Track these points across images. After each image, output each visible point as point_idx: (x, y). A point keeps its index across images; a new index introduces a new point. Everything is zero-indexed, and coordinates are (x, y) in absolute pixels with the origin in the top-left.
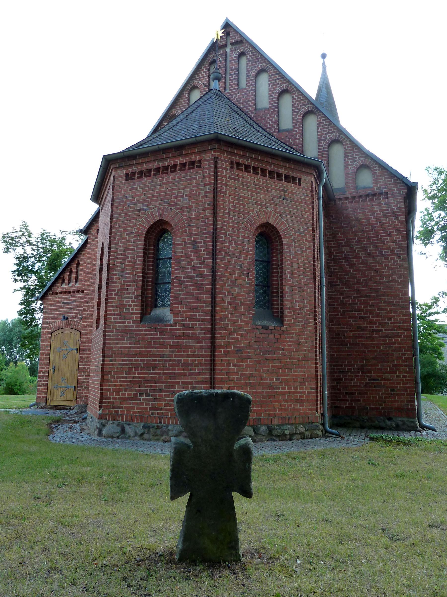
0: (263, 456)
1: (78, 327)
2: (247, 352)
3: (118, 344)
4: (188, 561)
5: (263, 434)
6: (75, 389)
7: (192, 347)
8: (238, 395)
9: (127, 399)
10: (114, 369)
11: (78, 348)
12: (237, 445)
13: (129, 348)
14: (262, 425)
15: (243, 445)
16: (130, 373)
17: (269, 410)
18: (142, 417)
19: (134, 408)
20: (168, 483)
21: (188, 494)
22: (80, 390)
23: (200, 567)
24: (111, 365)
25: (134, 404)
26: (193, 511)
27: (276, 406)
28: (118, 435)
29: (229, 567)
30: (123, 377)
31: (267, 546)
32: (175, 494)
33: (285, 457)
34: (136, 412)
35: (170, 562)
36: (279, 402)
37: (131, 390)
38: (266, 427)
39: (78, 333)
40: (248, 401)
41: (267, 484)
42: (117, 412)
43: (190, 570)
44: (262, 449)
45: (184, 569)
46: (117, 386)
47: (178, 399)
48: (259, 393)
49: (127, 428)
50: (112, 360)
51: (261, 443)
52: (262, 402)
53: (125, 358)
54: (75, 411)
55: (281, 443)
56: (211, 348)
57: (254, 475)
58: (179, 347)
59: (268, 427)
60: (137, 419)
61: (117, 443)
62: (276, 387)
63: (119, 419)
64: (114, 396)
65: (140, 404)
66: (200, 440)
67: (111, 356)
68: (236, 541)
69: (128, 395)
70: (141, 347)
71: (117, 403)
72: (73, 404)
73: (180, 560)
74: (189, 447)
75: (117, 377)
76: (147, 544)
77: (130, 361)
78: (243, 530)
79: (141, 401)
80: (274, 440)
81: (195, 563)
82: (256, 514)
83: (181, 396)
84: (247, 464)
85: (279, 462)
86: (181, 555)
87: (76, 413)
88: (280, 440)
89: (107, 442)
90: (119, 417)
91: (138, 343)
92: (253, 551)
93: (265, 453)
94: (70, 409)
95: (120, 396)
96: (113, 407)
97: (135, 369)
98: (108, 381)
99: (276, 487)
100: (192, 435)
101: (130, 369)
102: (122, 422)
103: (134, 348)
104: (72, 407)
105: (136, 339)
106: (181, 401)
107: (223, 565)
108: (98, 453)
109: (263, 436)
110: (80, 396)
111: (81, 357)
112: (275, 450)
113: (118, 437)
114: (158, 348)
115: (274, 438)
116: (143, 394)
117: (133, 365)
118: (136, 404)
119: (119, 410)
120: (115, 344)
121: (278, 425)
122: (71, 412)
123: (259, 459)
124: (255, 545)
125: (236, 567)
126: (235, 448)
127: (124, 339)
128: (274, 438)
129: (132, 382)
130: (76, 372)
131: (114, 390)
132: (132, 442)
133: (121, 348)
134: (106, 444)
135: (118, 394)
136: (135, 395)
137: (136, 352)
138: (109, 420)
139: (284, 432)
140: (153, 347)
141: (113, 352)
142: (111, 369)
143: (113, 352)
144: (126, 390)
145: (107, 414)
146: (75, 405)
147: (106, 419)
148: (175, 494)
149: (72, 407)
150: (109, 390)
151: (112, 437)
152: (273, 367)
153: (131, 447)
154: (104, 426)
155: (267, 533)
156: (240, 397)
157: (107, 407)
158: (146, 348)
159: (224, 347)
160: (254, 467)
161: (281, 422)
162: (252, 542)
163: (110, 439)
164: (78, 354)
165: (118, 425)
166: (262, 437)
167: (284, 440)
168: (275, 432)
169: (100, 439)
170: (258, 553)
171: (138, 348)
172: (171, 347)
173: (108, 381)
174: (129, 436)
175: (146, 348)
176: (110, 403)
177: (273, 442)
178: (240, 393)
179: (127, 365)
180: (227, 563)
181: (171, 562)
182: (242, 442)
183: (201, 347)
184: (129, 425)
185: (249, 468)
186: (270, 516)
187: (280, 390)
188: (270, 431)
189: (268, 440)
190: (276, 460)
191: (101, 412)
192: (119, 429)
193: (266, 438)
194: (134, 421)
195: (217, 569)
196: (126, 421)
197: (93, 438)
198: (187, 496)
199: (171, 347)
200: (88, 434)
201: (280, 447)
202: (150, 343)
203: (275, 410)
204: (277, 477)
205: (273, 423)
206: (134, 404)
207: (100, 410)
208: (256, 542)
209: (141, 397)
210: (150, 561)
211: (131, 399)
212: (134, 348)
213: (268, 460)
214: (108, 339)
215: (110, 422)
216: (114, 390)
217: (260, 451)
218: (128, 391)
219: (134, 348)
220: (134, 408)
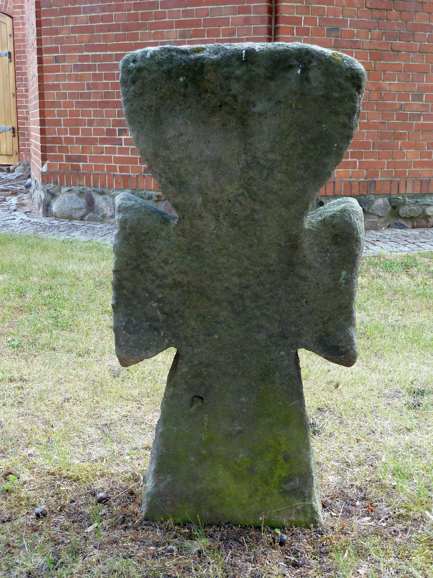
0: (379, 257)
1: (6, 7)
2: (352, 34)
3: (67, 21)
4: (170, 522)
5: (380, 214)
6: (14, 132)
7: (225, 22)
8: (319, 57)
9: (93, 141)
10: (64, 77)
11: (12, 51)
12: (312, 219)
13: (89, 30)
14: (378, 195)
15: (333, 217)
16: (95, 86)
17: (394, 165)
18: (126, 179)
19: (108, 160)
20: (108, 320)
21: (172, 352)
22: (23, 134)
23: (201, 543)
24: (57, 69)
25: (109, 150)
26: (186, 395)
27: (411, 155)
28: (81, 213)
29: (282, 543)
30: (82, 95)
31: (389, 480)
32: (132, 346)
33: (427, 260)
34: (114, 169)
35: (123, 521)
36: (417, 147)
37: (102, 123)
38: (386, 199)
39: (8, 20)
40: (355, 79)
41: (386, 317)
42: (77, 168)
43: (171, 551)
44: (376, 243)
45: (157, 545)
46: (72, 113)
47: (127, 71)
48: (374, 126)
49: (99, 200)
50: (57, 60)
51: (374, 232)
52: (381, 146)
53: (85, 53)
54: (17, 173)
55: (416, 232)
56: (270, 22)
57: (360, 296)
58: (197, 23)
59: (390, 200)
60: (117, 183)
61: (77, 228)
62: (413, 115)
63: (81, 184)
64: (68, 136)
65: (122, 151)
66: (199, 200)
67: (56, 50)
68: (306, 477)
69: (97, 132)
70: (117, 28)
71: (76, 150)
72: (13, 161)
73: (149, 520)
74: (165, 220)
75: (72, 96)
76: (77, 464)
77: (95, 58)
78: (329, 429)
79: (124, 146)
80: (402, 227)
81: (186, 528)
82: (361, 388)
83: (134, 61)
84: (344, 273)
85: (414, 271)
86: (151, 506)
87: (18, 178)
88: (414, 227)
89: (58, 227)
90: (81, 179)
91: (109, 18)
92: (352, 493)
93: (384, 252)
94: (9, 171)
95: (80, 136)
96: (69, 159)
97: (107, 77)
98: (53, 104)
99: (408, 323)
100: (174, 183)
101: (97, 77)
102: (89, 189)
103: (101, 31)
104: (11, 168)
105: (103, 9)
106: (137, 77)
107: (266, 537)
108: (32, 247)
109: (379, 217)
110: (24, 145)
111: (18, 69)
112: (405, 245)
113: (82, 219)
114: (152, 26)
115: (403, 222)
116: (125, 130)
117: (101, 67)
118: (112, 151)
119: (81, 164)
120: (62, 22)
121: (412, 196)
122: (9, 176)
123: (370, 263)
124: (358, 475)
125: (303, 544)
126: (306, 226)
127: (78, 11)
128: (403, 222)
129: (103, 104)
130: (13, 100)
131: (67, 123)
132: (109, 226)
133: (74, 30)
134: (55, 231)
135: (76, 132)
136: (110, 132)
137: (105, 38)
138: (62, 184)
139: (424, 211)
140: (140, 26)
141: (57, 41)
142: (57, 78)
143: (57, 41)
144: (90, 123)
145: (58, 173)
146: (17, 163)
147: (56, 183)
148: (132, 346)
149: (11, 168)
150: (58, 123)
151: (70, 218)
152: (408, 68)
153: (104, 238)
154: (54, 196)
155: (390, 441)
156: (328, 65)
157: (55, 158)
158: (126, 28)
159: (298, 21)
160: (360, 280)
161: (419, 189)
162: (348, 465)
163: (66, 222)
164: (12, 64)
165: (81, 194)
166: (376, 220)
167: (423, 227)
168: (403, 211)
169: (45, 221)
170: (363, 499)
171: (110, 28)
172: (179, 24)
173: (53, 104)
174: (104, 216)
175: (126, 28)
176: (61, 149)
177: (399, 230)
178: (329, 52)
179: (89, 68)
180: (278, 531)
181: (124, 521)
182: (332, 207)
183: (247, 21)
184: (102, 193)
185: (350, 282)
186: (397, 394)
187: (422, 121)
188: (395, 208)
189: (389, 227)
190: (407, 267)
191: (45, 169)
192: (82, 202)
193: (386, 222)
194: (111, 186)
195: (250, 548)
196: (95, 186)
197: (33, 220)
198: (165, 358)
199: (179, 24)
200: (26, 213)
201: (414, 241)
202: (134, 17)
203: (407, 165)
204: (410, 302)
205: (402, 191)
206: (109, 150)
207: (43, 164)
208: (360, 464)
209: (123, 137)
210: (69, 516)
211: (103, 141)
212: (101, 29)
213: (388, 266)
214: (47, 13)
215: (64, 189)
216: (67, 123)
217: (371, 246)
218: (95, 124)
219: (101, 29)
220: (108, 160)
